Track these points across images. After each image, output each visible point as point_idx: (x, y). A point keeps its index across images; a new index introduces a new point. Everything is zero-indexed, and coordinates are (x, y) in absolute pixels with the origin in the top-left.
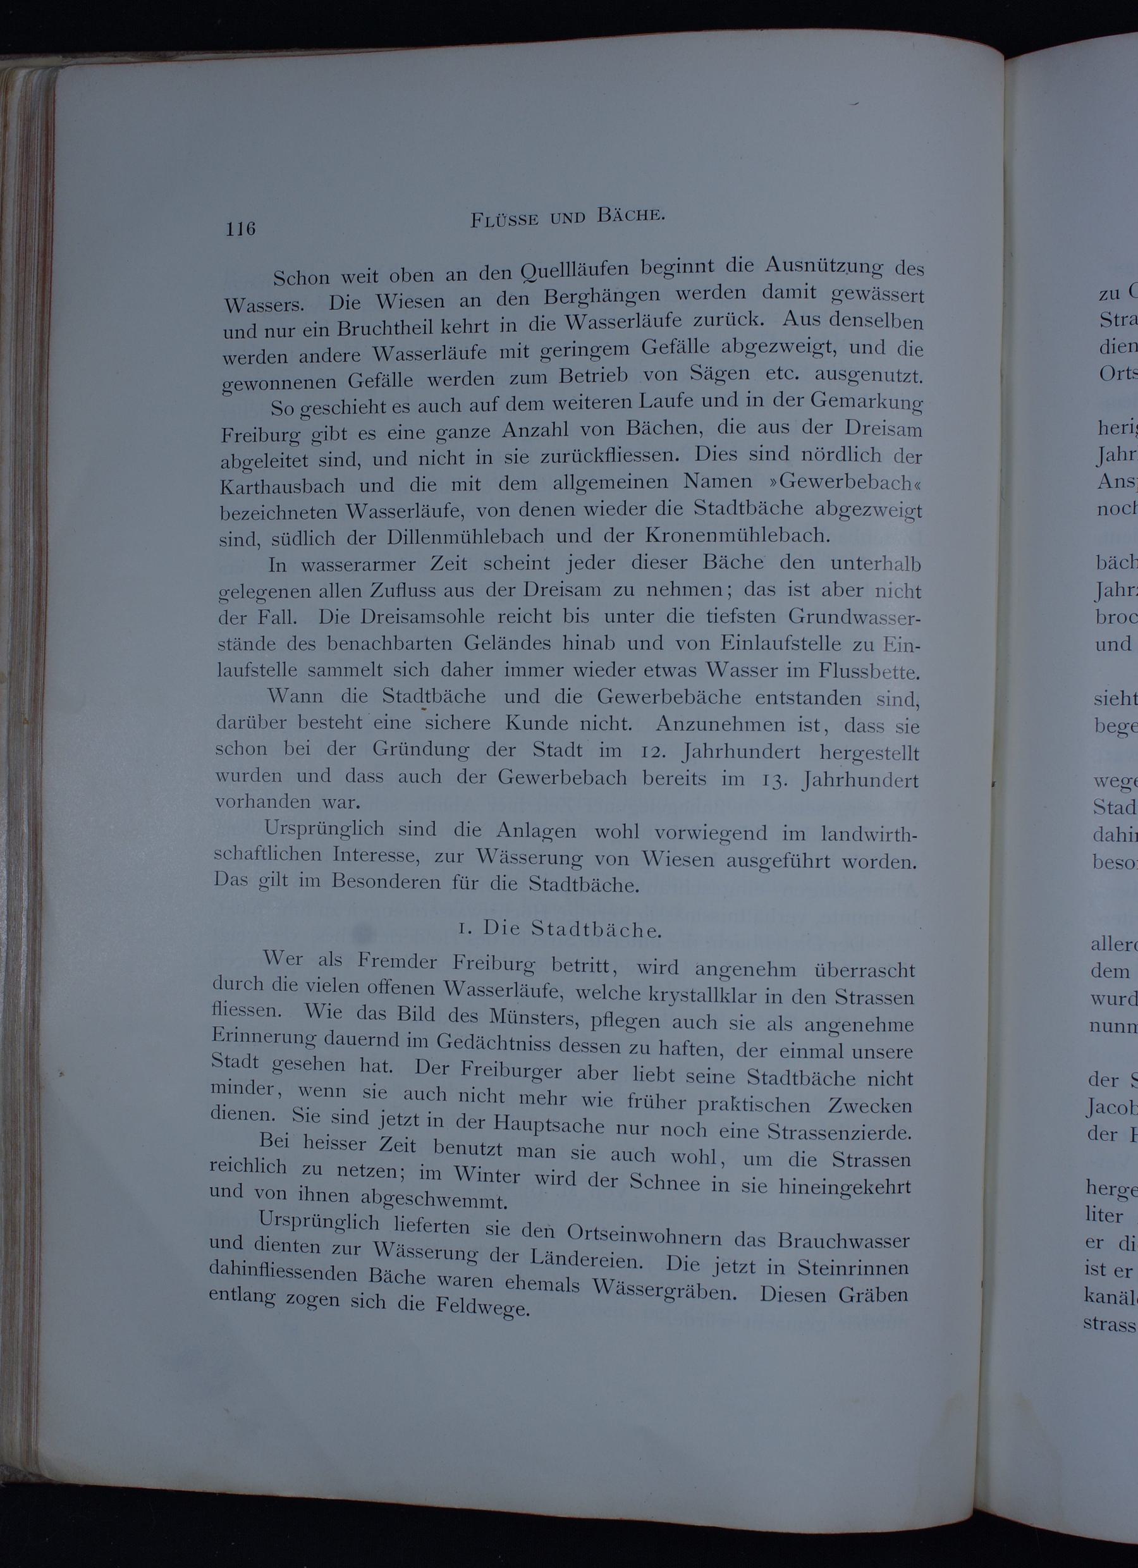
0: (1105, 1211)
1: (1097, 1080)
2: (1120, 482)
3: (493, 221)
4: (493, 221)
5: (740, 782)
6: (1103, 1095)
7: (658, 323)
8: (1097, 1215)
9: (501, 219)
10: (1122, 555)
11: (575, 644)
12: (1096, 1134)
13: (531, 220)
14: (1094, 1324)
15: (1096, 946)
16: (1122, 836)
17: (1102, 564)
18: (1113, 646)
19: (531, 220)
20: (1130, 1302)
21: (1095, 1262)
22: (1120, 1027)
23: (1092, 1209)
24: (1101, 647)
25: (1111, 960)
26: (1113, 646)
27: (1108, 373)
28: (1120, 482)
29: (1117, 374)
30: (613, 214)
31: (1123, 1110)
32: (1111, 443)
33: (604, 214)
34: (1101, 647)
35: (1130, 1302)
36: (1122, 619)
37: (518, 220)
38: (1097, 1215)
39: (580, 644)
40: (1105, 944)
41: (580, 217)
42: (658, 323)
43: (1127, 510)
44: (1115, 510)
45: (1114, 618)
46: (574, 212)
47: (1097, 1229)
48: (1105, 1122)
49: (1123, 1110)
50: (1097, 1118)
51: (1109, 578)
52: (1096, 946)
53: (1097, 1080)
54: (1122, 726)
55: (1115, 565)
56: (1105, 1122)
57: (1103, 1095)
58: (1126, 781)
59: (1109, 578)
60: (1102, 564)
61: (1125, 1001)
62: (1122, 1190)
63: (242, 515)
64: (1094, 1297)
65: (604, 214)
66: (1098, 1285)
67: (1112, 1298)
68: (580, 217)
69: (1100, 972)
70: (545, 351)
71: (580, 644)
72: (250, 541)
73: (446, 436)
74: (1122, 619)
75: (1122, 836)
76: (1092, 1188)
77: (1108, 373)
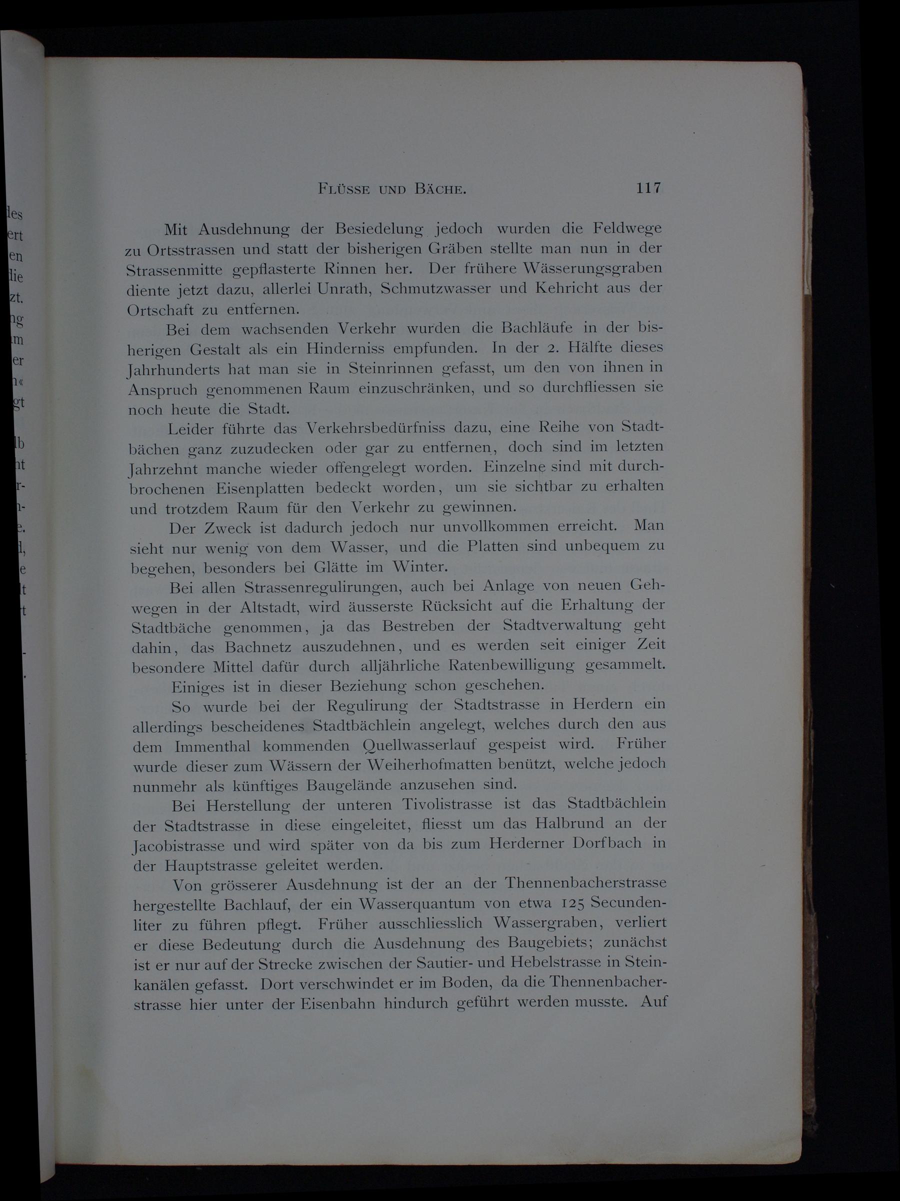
0: (148, 923)
1: (140, 827)
2: (145, 391)
3: (335, 189)
4: (335, 189)
5: (476, 846)
6: (145, 838)
7: (555, 330)
8: (142, 926)
9: (342, 188)
10: (148, 444)
11: (158, 649)
12: (140, 867)
13: (364, 190)
14: (142, 1006)
15: (136, 730)
16: (153, 649)
17: (133, 451)
18: (143, 511)
19: (364, 190)
20: (168, 987)
21: (142, 960)
22: (156, 787)
23: (138, 922)
24: (134, 511)
25: (148, 739)
26: (143, 511)
27: (133, 310)
28: (145, 391)
29: (140, 311)
30: (427, 188)
31: (159, 848)
32: (138, 362)
33: (420, 188)
34: (134, 511)
35: (168, 987)
36: (149, 491)
37: (354, 190)
38: (142, 926)
39: (162, 649)
40: (143, 728)
41: (402, 190)
42: (555, 330)
43: (151, 411)
44: (142, 411)
45: (143, 491)
46: (397, 185)
47: (143, 936)
48: (146, 857)
49: (159, 848)
50: (141, 855)
51: (139, 461)
52: (136, 730)
53: (140, 827)
54: (152, 569)
55: (143, 451)
56: (146, 857)
57: (145, 838)
58: (155, 609)
59: (139, 461)
60: (133, 451)
61: (159, 768)
62: (160, 906)
63: (350, 687)
64: (142, 987)
65: (420, 188)
66: (144, 977)
67: (155, 986)
68: (402, 190)
69: (140, 748)
70: (446, 368)
71: (162, 649)
72: (508, 785)
73: (196, 453)
74: (149, 491)
75: (153, 649)
76: (138, 906)
77: (133, 310)
